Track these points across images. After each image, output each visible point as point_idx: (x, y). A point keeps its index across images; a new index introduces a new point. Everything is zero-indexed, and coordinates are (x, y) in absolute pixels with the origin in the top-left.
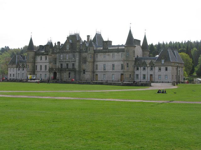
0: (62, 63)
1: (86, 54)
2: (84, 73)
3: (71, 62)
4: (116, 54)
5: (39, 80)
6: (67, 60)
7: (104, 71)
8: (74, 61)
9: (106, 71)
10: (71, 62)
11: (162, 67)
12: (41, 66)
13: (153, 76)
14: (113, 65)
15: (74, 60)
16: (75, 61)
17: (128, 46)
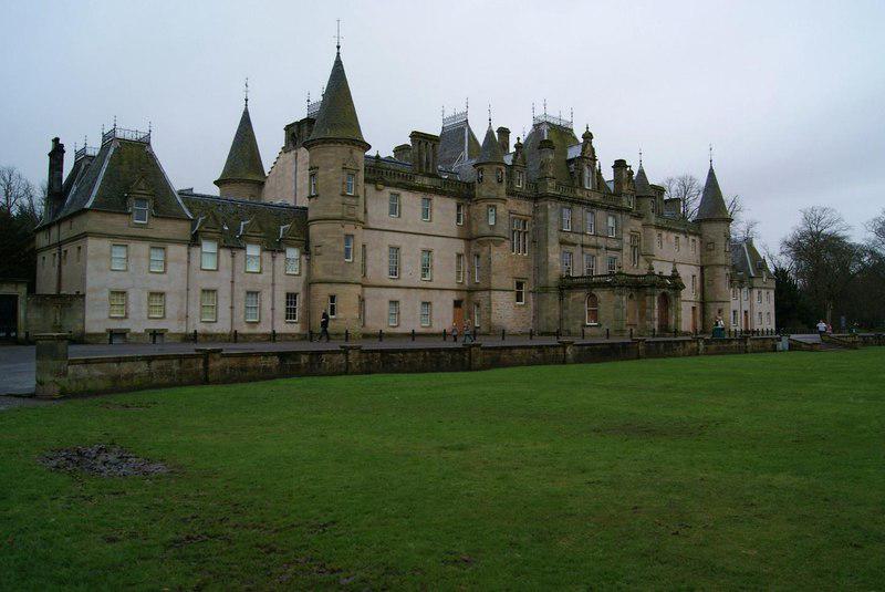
16: (619, 250)
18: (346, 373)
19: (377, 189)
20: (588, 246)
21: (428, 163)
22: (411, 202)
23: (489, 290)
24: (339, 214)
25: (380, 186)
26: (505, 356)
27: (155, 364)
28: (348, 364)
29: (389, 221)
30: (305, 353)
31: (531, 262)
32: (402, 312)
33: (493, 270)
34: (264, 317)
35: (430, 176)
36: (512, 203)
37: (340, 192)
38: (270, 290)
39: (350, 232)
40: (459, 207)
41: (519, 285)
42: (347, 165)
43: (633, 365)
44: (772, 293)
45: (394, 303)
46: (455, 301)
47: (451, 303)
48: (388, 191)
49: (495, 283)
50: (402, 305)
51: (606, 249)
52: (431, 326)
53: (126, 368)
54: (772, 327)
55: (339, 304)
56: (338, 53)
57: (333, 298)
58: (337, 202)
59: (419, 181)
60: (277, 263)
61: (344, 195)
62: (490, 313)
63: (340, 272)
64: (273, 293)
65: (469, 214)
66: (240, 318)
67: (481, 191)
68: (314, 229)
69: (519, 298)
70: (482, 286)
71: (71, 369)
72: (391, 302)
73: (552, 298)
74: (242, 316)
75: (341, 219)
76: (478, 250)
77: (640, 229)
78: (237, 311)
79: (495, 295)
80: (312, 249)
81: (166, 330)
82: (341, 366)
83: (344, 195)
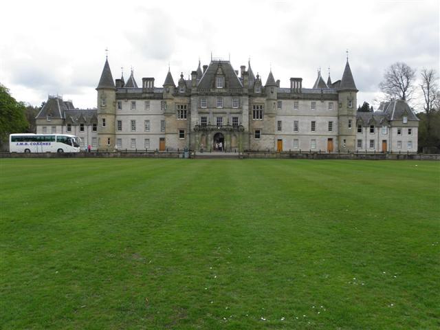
0: (204, 116)
1: (263, 100)
2: (258, 136)
3: (231, 113)
4: (318, 102)
5: (76, 146)
6: (217, 111)
8: (237, 113)
10: (231, 113)
11: (404, 129)
12: (133, 122)
13: (388, 143)
14: (313, 123)
15: (238, 111)
16: (240, 113)
17: (103, 89)
20: (216, 113)
44: (415, 131)
45: (133, 140)
69: (182, 136)
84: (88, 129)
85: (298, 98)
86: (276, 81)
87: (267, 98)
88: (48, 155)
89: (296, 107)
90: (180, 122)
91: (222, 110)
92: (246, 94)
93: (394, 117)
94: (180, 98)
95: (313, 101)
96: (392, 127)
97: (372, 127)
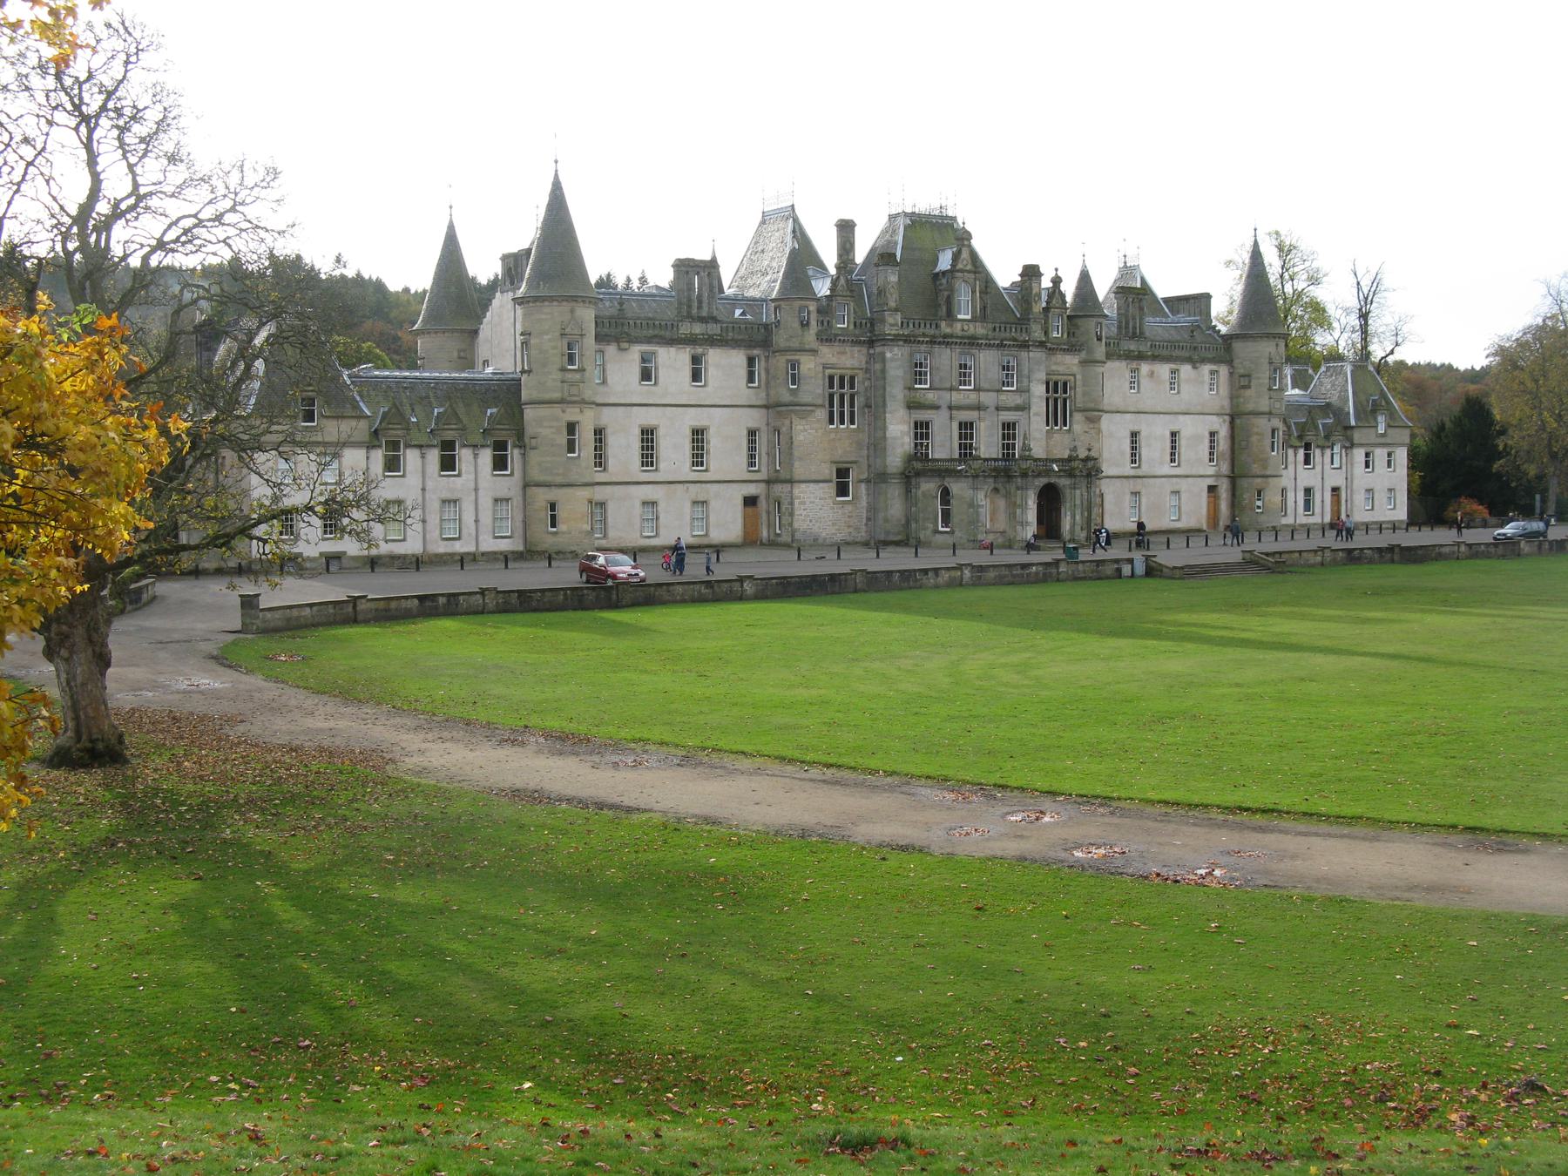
7: (1132, 472)
9: (1145, 469)
12: (648, 436)
15: (1018, 400)
16: (1024, 408)
18: (482, 613)
19: (620, 349)
20: (960, 408)
21: (700, 302)
22: (673, 362)
23: (791, 481)
24: (556, 395)
25: (625, 345)
26: (662, 592)
27: (315, 608)
28: (485, 604)
29: (640, 393)
30: (442, 595)
31: (864, 437)
32: (662, 517)
33: (796, 453)
34: (464, 532)
35: (702, 320)
36: (828, 354)
37: (559, 366)
38: (473, 498)
39: (573, 418)
40: (751, 361)
41: (842, 473)
42: (568, 330)
43: (1488, 562)
44: (1402, 455)
46: (745, 498)
47: (740, 502)
48: (636, 351)
49: (799, 470)
50: (661, 507)
51: (997, 409)
52: (706, 535)
53: (295, 613)
54: (1401, 514)
55: (561, 513)
56: (556, 171)
57: (553, 507)
58: (554, 380)
59: (685, 329)
60: (480, 461)
61: (563, 370)
62: (792, 514)
63: (561, 471)
64: (476, 500)
65: (767, 371)
66: (434, 533)
67: (780, 339)
68: (529, 413)
69: (842, 490)
70: (783, 475)
71: (261, 614)
72: (644, 503)
73: (894, 493)
74: (438, 532)
75: (561, 401)
76: (778, 423)
77: (1075, 369)
78: (429, 526)
79: (799, 490)
80: (527, 440)
81: (345, 553)
82: (478, 605)
83: (563, 370)
84: (475, 464)
85: (1141, 357)
86: (593, 279)
87: (1083, 355)
88: (748, 587)
89: (1134, 383)
90: (841, 441)
91: (973, 398)
92: (896, 339)
93: (1357, 417)
94: (837, 348)
95: (1173, 366)
96: (1352, 445)
97: (448, 446)
